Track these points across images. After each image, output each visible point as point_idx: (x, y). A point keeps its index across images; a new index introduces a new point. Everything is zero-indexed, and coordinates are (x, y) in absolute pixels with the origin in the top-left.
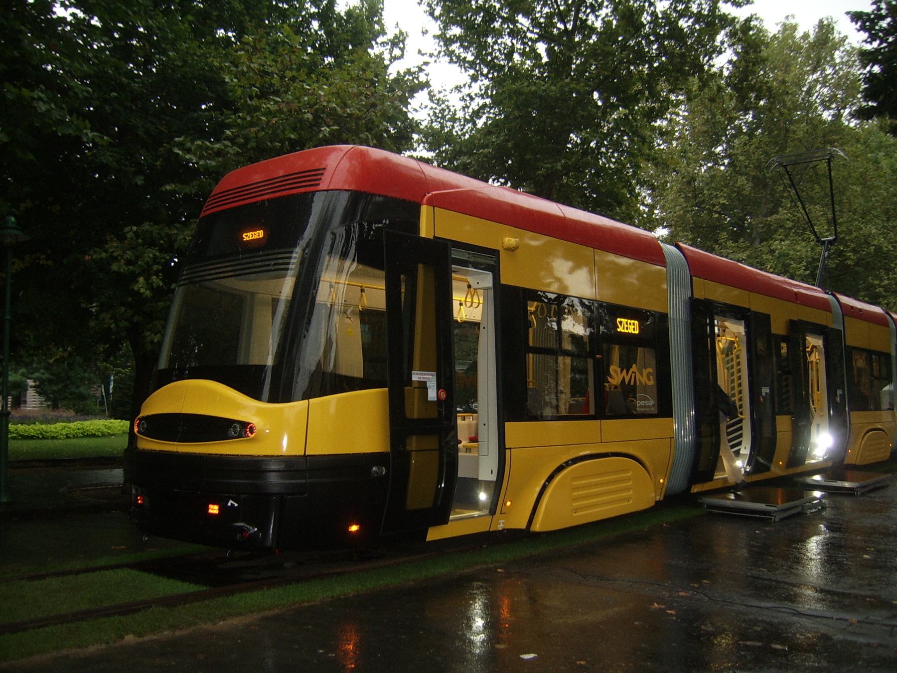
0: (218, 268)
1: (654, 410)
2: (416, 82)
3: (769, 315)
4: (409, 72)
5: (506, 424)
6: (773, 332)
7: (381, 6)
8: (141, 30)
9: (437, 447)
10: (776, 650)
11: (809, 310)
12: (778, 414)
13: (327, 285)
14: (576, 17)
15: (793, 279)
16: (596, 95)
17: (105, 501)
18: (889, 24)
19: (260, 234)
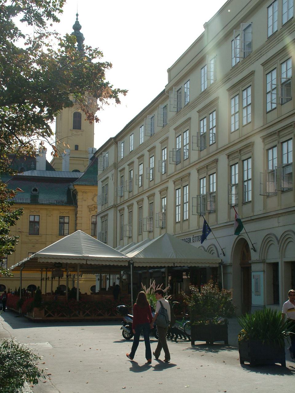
0: (203, 97)
1: (29, 201)
2: (35, 70)
3: (130, 370)
4: (16, 29)
5: (195, 344)
6: (195, 342)
7: (262, 367)
8: (224, 309)
9: (196, 143)
10: (231, 191)
11: (268, 71)
12: (52, 273)
13: (127, 238)
14: (85, 111)
15: (131, 292)
16: (6, 89)
17: (222, 348)
18: (5, 86)
19: (280, 365)
